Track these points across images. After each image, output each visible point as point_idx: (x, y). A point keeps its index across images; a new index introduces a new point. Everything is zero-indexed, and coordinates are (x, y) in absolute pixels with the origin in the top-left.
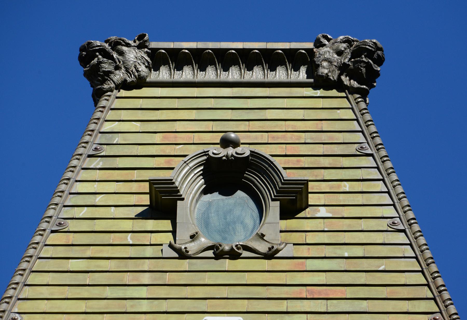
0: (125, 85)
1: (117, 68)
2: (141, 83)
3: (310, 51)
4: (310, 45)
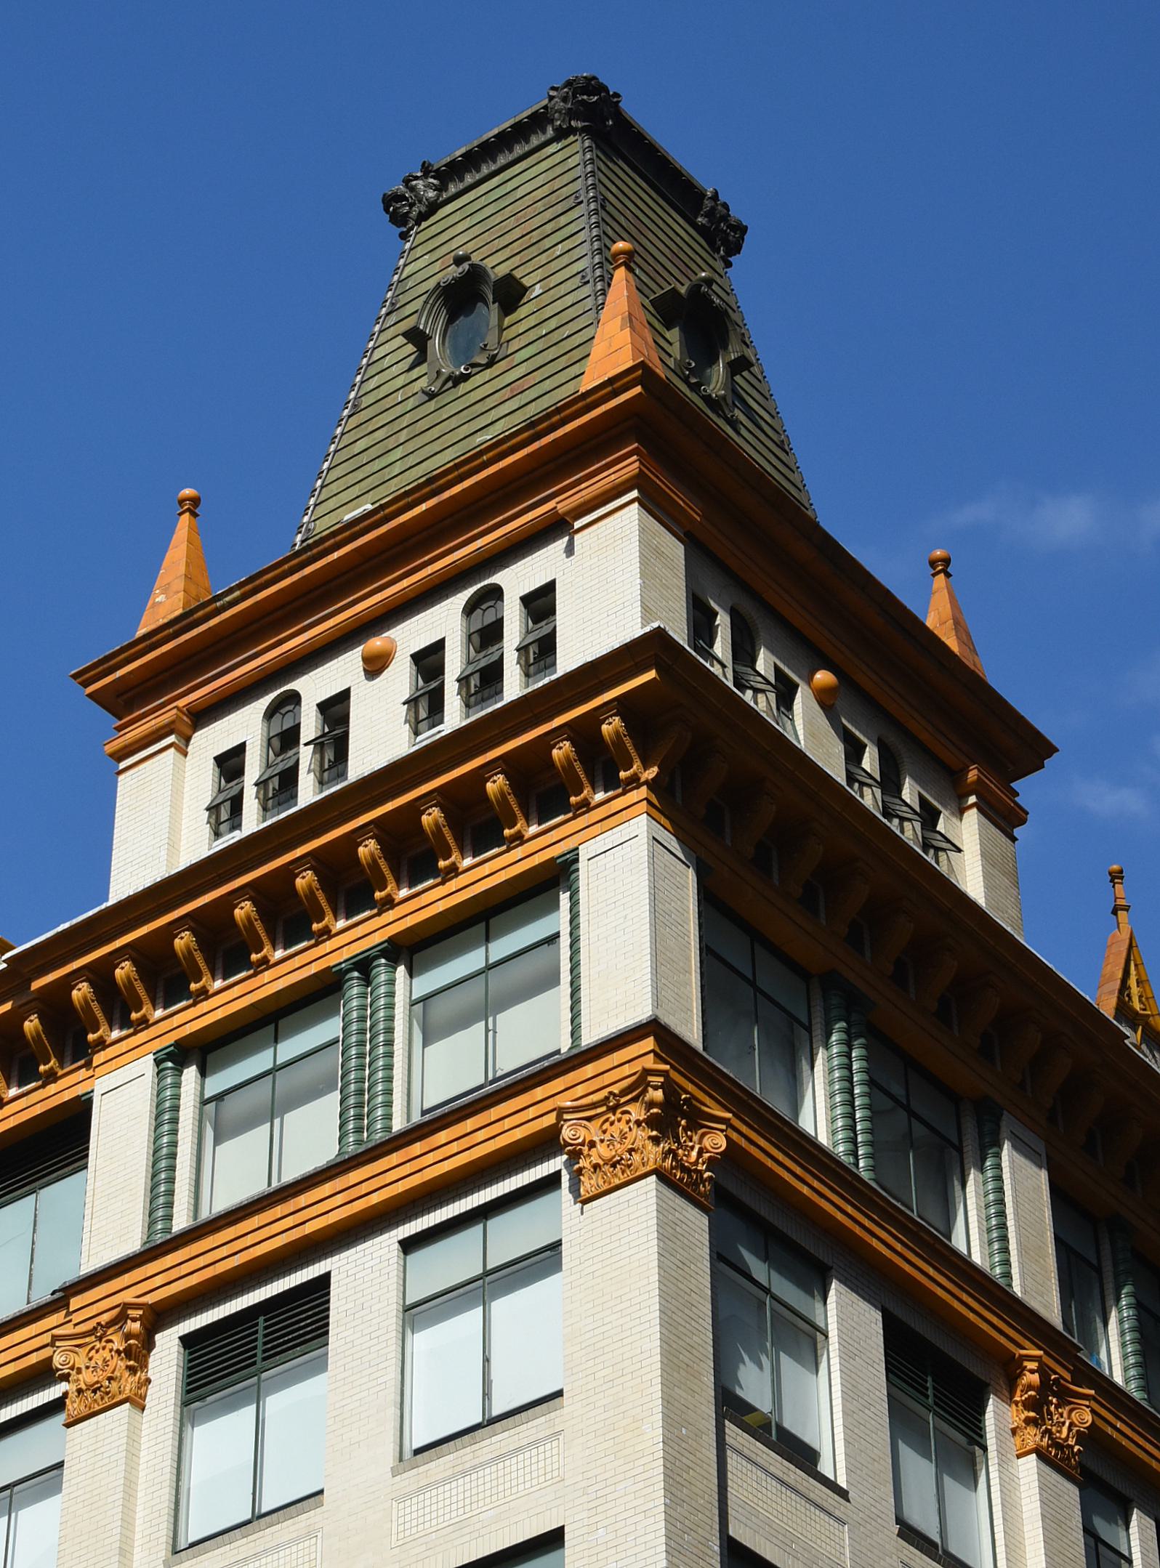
0: (423, 217)
1: (411, 205)
2: (434, 207)
3: (545, 107)
4: (546, 102)
